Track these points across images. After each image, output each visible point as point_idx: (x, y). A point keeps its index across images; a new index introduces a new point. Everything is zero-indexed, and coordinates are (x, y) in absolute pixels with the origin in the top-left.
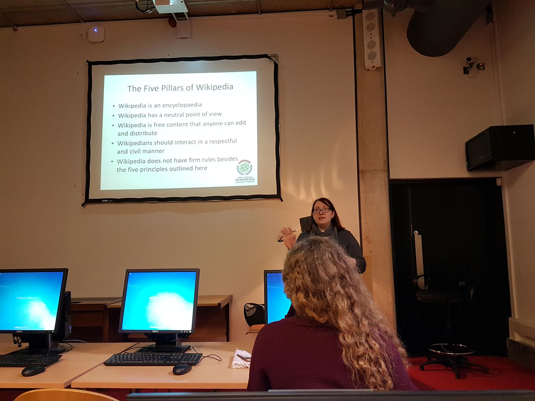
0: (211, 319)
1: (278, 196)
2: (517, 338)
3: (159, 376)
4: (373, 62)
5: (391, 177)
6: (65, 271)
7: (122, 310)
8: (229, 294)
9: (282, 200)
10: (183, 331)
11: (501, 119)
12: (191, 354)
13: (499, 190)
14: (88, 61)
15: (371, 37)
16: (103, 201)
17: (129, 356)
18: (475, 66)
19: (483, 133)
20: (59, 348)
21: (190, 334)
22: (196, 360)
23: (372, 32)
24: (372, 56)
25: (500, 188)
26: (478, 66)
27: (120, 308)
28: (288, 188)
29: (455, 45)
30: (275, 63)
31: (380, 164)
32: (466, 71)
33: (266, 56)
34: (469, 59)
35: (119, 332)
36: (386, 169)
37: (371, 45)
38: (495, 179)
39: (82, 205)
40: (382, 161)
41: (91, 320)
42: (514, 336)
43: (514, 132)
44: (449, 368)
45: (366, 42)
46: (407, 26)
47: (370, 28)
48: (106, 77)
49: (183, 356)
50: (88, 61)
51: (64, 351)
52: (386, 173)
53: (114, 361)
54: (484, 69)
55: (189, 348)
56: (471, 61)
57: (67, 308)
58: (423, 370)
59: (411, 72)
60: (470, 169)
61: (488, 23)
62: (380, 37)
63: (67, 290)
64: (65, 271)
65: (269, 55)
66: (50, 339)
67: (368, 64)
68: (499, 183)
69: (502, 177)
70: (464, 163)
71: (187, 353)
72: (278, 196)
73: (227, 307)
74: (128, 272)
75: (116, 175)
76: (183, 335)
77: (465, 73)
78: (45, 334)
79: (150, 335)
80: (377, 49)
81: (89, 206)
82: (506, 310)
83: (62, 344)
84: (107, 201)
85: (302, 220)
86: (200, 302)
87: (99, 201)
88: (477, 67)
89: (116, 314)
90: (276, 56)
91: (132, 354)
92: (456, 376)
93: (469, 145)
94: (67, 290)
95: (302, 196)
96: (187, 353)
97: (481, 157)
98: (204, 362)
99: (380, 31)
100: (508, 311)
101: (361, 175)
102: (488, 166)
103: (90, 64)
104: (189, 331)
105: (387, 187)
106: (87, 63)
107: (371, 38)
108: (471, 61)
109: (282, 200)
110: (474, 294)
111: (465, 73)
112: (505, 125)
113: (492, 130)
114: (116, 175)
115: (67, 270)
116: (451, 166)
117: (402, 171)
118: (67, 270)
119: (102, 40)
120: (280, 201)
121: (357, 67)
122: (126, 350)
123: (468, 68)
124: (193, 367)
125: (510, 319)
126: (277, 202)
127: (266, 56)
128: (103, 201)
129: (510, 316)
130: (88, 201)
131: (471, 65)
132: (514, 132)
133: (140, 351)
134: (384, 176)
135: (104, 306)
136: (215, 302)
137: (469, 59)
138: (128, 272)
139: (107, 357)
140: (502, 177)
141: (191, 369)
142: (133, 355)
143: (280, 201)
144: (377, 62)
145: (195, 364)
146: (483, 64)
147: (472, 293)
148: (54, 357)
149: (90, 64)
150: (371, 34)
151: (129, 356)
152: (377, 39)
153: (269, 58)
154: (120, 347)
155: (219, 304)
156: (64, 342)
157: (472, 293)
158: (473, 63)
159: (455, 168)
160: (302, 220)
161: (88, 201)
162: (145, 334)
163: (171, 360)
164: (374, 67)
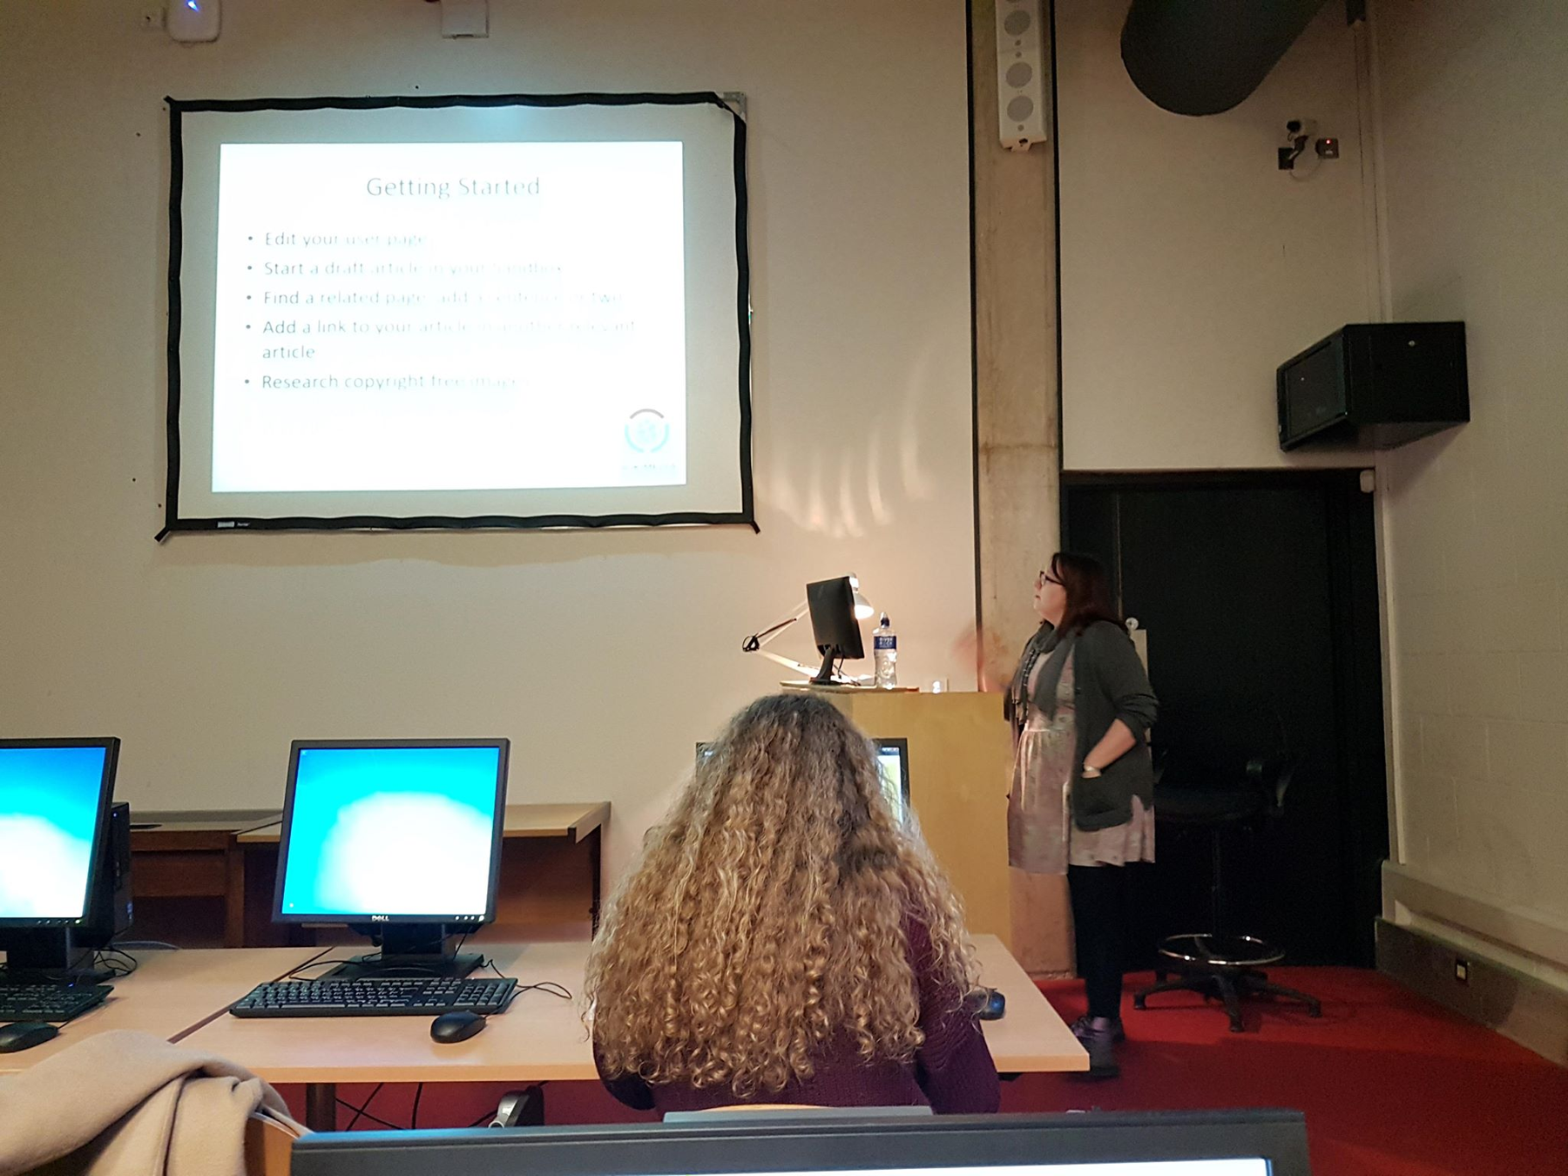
0: (546, 871)
1: (746, 518)
2: (1403, 917)
3: (390, 1049)
4: (1021, 128)
5: (1069, 465)
6: (111, 747)
7: (281, 851)
8: (602, 799)
9: (757, 530)
10: (462, 917)
11: (1377, 305)
12: (485, 982)
13: (1366, 504)
14: (168, 99)
15: (1018, 53)
16: (220, 525)
17: (304, 991)
18: (1310, 146)
19: (1325, 344)
20: (99, 968)
21: (481, 924)
22: (501, 998)
23: (1022, 37)
24: (1020, 109)
25: (1370, 497)
26: (1320, 147)
27: (277, 845)
28: (773, 494)
29: (1252, 89)
30: (737, 118)
31: (1038, 427)
32: (1285, 160)
33: (710, 97)
34: (1294, 126)
35: (274, 918)
36: (1054, 442)
37: (1019, 76)
38: (1355, 473)
39: (158, 538)
40: (1044, 421)
41: (184, 883)
42: (1394, 914)
43: (1412, 343)
44: (1214, 1001)
45: (1004, 64)
46: (1122, 22)
47: (1017, 24)
48: (226, 149)
49: (458, 991)
50: (168, 99)
51: (111, 974)
52: (1054, 455)
53: (259, 1005)
54: (1336, 155)
55: (478, 963)
56: (1302, 132)
57: (119, 844)
58: (1145, 1008)
59: (1133, 161)
60: (1289, 442)
61: (1351, 22)
62: (1044, 48)
63: (117, 798)
64: (111, 747)
65: (721, 96)
66: (68, 941)
67: (1008, 132)
68: (1366, 483)
69: (1377, 468)
70: (1273, 428)
71: (473, 977)
72: (746, 518)
73: (596, 837)
74: (297, 748)
75: (254, 448)
76: (464, 928)
77: (1281, 167)
78: (55, 929)
79: (360, 928)
80: (1035, 90)
81: (178, 541)
82: (1374, 836)
83: (105, 954)
84: (232, 524)
85: (813, 590)
86: (512, 826)
87: (209, 526)
88: (1317, 150)
89: (264, 862)
90: (740, 98)
91: (312, 982)
92: (1233, 1023)
93: (1286, 375)
94: (117, 798)
95: (816, 517)
96: (473, 977)
97: (1318, 411)
98: (523, 1005)
99: (1044, 37)
100: (1380, 845)
101: (982, 459)
102: (1339, 434)
103: (177, 109)
104: (477, 917)
105: (1055, 495)
106: (167, 106)
107: (1019, 55)
108: (1302, 132)
109: (757, 530)
110: (1286, 797)
111: (1281, 167)
112: (1389, 320)
113: (1349, 330)
114: (254, 448)
115: (118, 741)
116: (1236, 435)
117: (1091, 452)
118: (118, 741)
119: (211, 34)
120: (750, 531)
121: (977, 140)
122: (294, 971)
123: (1290, 151)
124: (490, 1020)
125: (1385, 864)
126: (745, 532)
127: (710, 97)
128: (220, 525)
129: (1387, 856)
130: (175, 525)
131: (1301, 143)
132: (1412, 343)
133: (338, 972)
134: (1047, 461)
135: (230, 837)
136: (558, 824)
137: (1294, 126)
138: (297, 748)
139: (240, 990)
140: (1377, 468)
141: (484, 1026)
142: (318, 984)
143: (751, 531)
144: (1035, 128)
145: (500, 1009)
146: (1335, 142)
147: (1280, 794)
148: (89, 995)
149: (177, 109)
150: (1018, 43)
151: (304, 991)
152: (1034, 58)
153: (721, 104)
154: (274, 963)
155: (572, 831)
156: (112, 950)
157: (1280, 794)
158: (1305, 138)
159: (1244, 440)
160: (813, 590)
161: (175, 525)
162: (351, 925)
163: (425, 1000)
164: (1025, 141)
